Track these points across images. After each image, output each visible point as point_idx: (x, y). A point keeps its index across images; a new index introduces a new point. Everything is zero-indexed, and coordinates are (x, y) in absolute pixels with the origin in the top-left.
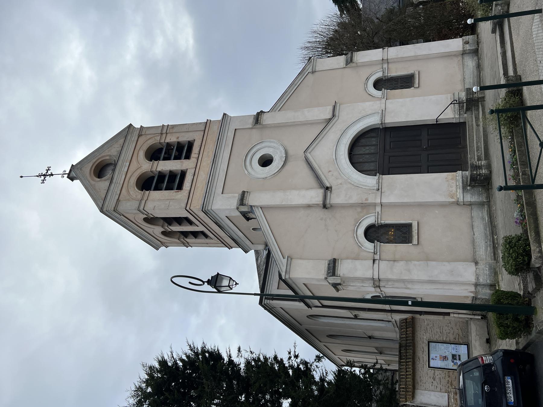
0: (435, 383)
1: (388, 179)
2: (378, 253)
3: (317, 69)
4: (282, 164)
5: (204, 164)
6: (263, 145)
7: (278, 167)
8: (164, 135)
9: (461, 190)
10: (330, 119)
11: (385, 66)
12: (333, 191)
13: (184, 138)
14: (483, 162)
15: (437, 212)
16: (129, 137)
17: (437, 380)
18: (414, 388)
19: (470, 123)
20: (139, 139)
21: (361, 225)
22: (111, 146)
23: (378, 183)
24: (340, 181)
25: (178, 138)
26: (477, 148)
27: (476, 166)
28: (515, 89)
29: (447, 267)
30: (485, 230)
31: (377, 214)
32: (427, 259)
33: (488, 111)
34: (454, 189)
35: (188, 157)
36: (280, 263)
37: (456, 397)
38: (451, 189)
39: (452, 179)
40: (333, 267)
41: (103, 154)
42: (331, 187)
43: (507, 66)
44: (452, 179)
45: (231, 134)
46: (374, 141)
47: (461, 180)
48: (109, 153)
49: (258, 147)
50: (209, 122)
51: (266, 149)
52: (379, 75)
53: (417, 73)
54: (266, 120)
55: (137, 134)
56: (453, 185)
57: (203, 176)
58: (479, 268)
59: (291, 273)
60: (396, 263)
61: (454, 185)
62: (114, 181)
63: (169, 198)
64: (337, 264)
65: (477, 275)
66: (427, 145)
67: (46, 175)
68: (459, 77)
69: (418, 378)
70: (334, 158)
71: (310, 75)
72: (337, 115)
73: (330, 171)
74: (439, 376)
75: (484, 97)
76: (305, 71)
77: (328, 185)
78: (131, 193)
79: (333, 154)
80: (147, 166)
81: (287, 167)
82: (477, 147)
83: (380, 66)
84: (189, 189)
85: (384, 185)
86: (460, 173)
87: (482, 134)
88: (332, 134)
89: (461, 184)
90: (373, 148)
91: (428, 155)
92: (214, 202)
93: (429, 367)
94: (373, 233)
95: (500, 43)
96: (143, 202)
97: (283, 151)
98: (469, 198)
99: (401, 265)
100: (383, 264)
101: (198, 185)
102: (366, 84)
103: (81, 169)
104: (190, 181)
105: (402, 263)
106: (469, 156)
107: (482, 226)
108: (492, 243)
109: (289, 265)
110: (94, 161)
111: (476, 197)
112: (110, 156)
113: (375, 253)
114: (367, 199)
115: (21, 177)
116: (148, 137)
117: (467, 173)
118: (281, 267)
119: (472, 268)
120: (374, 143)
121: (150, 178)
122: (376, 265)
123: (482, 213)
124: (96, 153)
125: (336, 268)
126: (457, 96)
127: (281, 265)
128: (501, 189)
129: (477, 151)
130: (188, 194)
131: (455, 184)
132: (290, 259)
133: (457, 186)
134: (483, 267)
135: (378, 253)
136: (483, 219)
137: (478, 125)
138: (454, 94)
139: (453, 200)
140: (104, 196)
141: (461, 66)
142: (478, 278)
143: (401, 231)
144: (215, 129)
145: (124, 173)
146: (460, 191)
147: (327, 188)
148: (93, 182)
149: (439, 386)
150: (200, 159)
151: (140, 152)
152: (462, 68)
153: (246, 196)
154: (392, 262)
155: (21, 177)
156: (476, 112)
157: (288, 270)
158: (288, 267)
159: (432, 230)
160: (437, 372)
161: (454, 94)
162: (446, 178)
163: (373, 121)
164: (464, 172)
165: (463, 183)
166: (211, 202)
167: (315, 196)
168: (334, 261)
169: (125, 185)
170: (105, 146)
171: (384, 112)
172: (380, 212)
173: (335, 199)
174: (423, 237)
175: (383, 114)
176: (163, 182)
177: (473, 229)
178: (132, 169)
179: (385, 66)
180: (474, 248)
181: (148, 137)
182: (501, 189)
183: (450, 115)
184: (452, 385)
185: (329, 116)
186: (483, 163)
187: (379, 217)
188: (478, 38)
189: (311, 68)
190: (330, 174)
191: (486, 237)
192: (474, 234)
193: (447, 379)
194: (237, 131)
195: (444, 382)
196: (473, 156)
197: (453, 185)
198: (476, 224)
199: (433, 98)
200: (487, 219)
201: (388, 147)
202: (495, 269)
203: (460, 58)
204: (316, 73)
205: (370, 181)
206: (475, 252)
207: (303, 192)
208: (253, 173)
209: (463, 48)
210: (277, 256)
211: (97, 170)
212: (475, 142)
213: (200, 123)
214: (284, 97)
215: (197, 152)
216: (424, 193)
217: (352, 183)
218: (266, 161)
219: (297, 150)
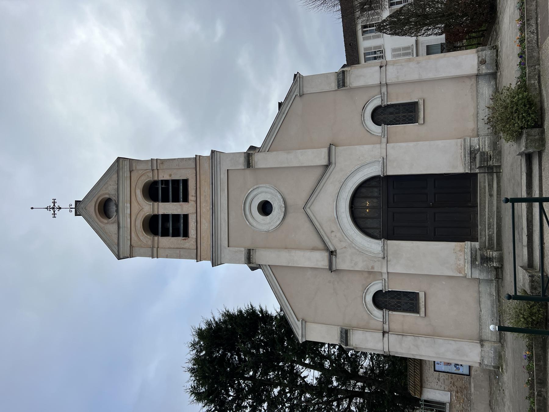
0: (440, 383)
2: (387, 323)
3: (305, 92)
4: (282, 215)
5: (204, 210)
6: (260, 190)
7: (279, 219)
8: (156, 171)
9: (469, 263)
10: (327, 167)
11: (384, 90)
12: (338, 256)
13: (178, 176)
14: (495, 254)
15: (444, 283)
16: (121, 173)
17: (441, 380)
18: (421, 387)
19: (482, 184)
20: (132, 175)
21: (369, 291)
22: (106, 183)
23: (384, 250)
24: (344, 244)
25: (170, 175)
26: (488, 225)
27: (487, 258)
28: (537, 87)
29: (454, 345)
30: (493, 307)
31: (384, 282)
32: (434, 334)
33: (503, 198)
34: (462, 262)
35: (186, 199)
36: (296, 326)
37: (457, 395)
38: (458, 262)
39: (460, 251)
40: (345, 334)
41: (101, 193)
42: (336, 251)
43: (532, 225)
44: (460, 251)
45: (224, 177)
46: (375, 192)
47: (469, 253)
48: (107, 191)
49: (255, 193)
50: (198, 158)
51: (263, 194)
52: (377, 102)
53: (421, 102)
54: (259, 160)
55: (128, 169)
56: (461, 257)
57: (205, 208)
58: (484, 351)
59: (307, 336)
60: (404, 337)
61: (462, 258)
62: (121, 225)
63: (178, 246)
64: (349, 335)
65: (482, 357)
67: (54, 208)
68: (471, 110)
69: (424, 378)
70: (336, 216)
71: (298, 99)
72: (333, 161)
73: (332, 232)
74: (443, 377)
75: (499, 167)
76: (292, 94)
78: (141, 238)
79: (333, 206)
80: (148, 208)
81: (289, 219)
83: (378, 90)
84: (195, 237)
85: (390, 252)
87: (495, 208)
88: (330, 187)
89: (469, 259)
91: (435, 214)
92: (222, 255)
93: (435, 371)
94: (383, 300)
95: (527, 186)
96: (155, 250)
97: (282, 200)
98: (477, 274)
99: (409, 340)
100: (393, 338)
101: (203, 235)
102: (363, 122)
103: (85, 208)
104: (194, 228)
105: (410, 338)
106: (479, 227)
107: (489, 303)
108: (498, 322)
109: (304, 328)
110: (95, 199)
111: (485, 274)
112: (109, 194)
113: (384, 323)
114: (373, 268)
115: (32, 208)
116: (140, 172)
117: (477, 245)
118: (297, 330)
119: (477, 349)
120: (376, 194)
121: (155, 206)
122: (386, 339)
123: (490, 288)
124: (94, 191)
125: (349, 338)
126: (469, 144)
127: (296, 328)
128: (509, 297)
129: (489, 229)
130: (195, 243)
131: (463, 257)
132: (304, 321)
133: (465, 259)
134: (488, 349)
135: (387, 323)
136: (491, 294)
137: (491, 195)
138: (465, 140)
139: (461, 275)
140: (116, 241)
141: (475, 93)
142: (483, 360)
143: (409, 297)
144: (206, 166)
145: (128, 216)
146: (468, 266)
148: (102, 225)
149: (443, 386)
150: (198, 169)
151: (137, 191)
152: (475, 96)
153: (252, 254)
154: (400, 337)
155: (32, 208)
156: (490, 177)
157: (304, 334)
158: (304, 331)
159: (440, 304)
160: (441, 374)
161: (465, 140)
164: (473, 243)
165: (471, 257)
166: (219, 256)
167: (320, 259)
168: (346, 332)
169: (133, 229)
170: (101, 184)
172: (387, 279)
173: (341, 263)
174: (430, 308)
176: (168, 221)
177: (480, 305)
178: (134, 212)
179: (384, 90)
180: (480, 325)
181: (140, 172)
182: (509, 297)
183: (460, 168)
184: (454, 385)
185: (325, 162)
186: (494, 255)
187: (387, 284)
188: (497, 55)
189: (297, 90)
190: (333, 234)
191: (493, 315)
192: (481, 311)
193: (450, 380)
194: (229, 171)
195: (447, 382)
196: (485, 231)
197: (461, 257)
198: (482, 300)
199: (439, 143)
200: (494, 294)
202: (500, 353)
203: (474, 81)
204: (304, 96)
205: (374, 246)
206: (481, 329)
207: (308, 254)
208: (254, 224)
209: (479, 70)
210: (292, 319)
211: (101, 208)
212: (487, 210)
213: (190, 159)
214: (273, 130)
215: (194, 195)
216: (429, 262)
217: (357, 248)
218: (265, 208)
219: (297, 198)
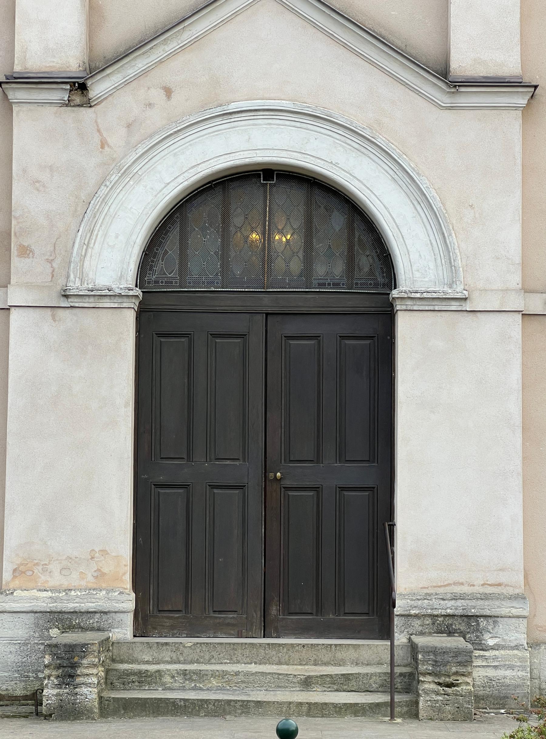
1: (121, 332)
10: (442, 73)
14: (89, 693)
23: (98, 297)
24: (117, 138)
26: (198, 673)
27: (74, 666)
38: (55, 567)
39: (100, 575)
42: (88, 104)
44: (100, 575)
46: (330, 268)
56: (75, 575)
61: (74, 580)
66: (287, 483)
70: (232, 107)
73: (168, 92)
75: (413, 713)
77: (98, 88)
82: (201, 675)
85: (88, 319)
86: (128, 602)
89: (70, 606)
90: (296, 266)
106: (189, 642)
114: (25, 251)
126: (504, 611)
129: (184, 673)
137: (307, 683)
146: (43, 601)
147: (83, 87)
162: (104, 552)
163: (416, 264)
171: (454, 306)
175: (443, 304)
185: (462, 63)
190: (157, 95)
196: (178, 661)
197: (75, 575)
201: (292, 327)
205: (113, 260)
212: (253, 668)
